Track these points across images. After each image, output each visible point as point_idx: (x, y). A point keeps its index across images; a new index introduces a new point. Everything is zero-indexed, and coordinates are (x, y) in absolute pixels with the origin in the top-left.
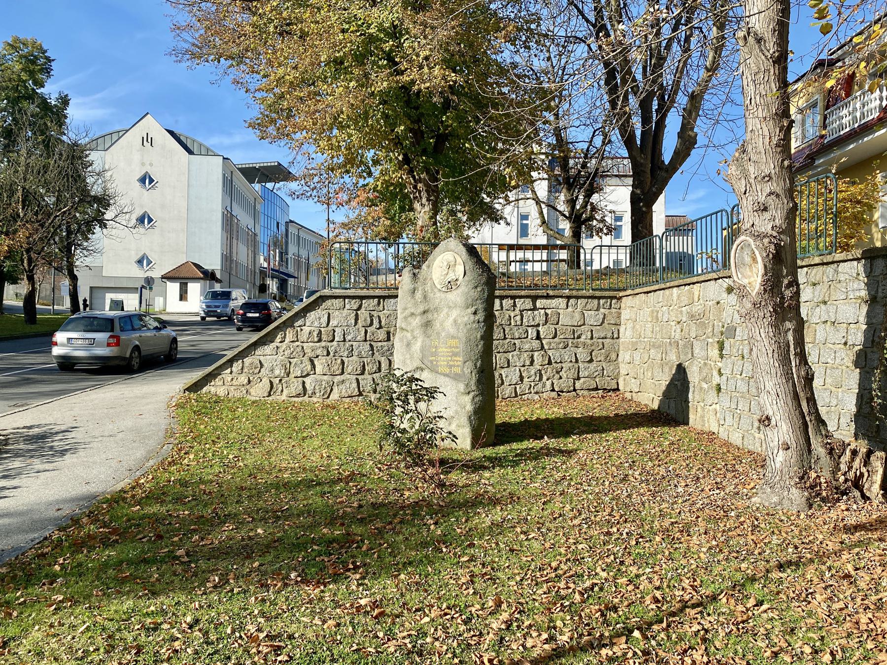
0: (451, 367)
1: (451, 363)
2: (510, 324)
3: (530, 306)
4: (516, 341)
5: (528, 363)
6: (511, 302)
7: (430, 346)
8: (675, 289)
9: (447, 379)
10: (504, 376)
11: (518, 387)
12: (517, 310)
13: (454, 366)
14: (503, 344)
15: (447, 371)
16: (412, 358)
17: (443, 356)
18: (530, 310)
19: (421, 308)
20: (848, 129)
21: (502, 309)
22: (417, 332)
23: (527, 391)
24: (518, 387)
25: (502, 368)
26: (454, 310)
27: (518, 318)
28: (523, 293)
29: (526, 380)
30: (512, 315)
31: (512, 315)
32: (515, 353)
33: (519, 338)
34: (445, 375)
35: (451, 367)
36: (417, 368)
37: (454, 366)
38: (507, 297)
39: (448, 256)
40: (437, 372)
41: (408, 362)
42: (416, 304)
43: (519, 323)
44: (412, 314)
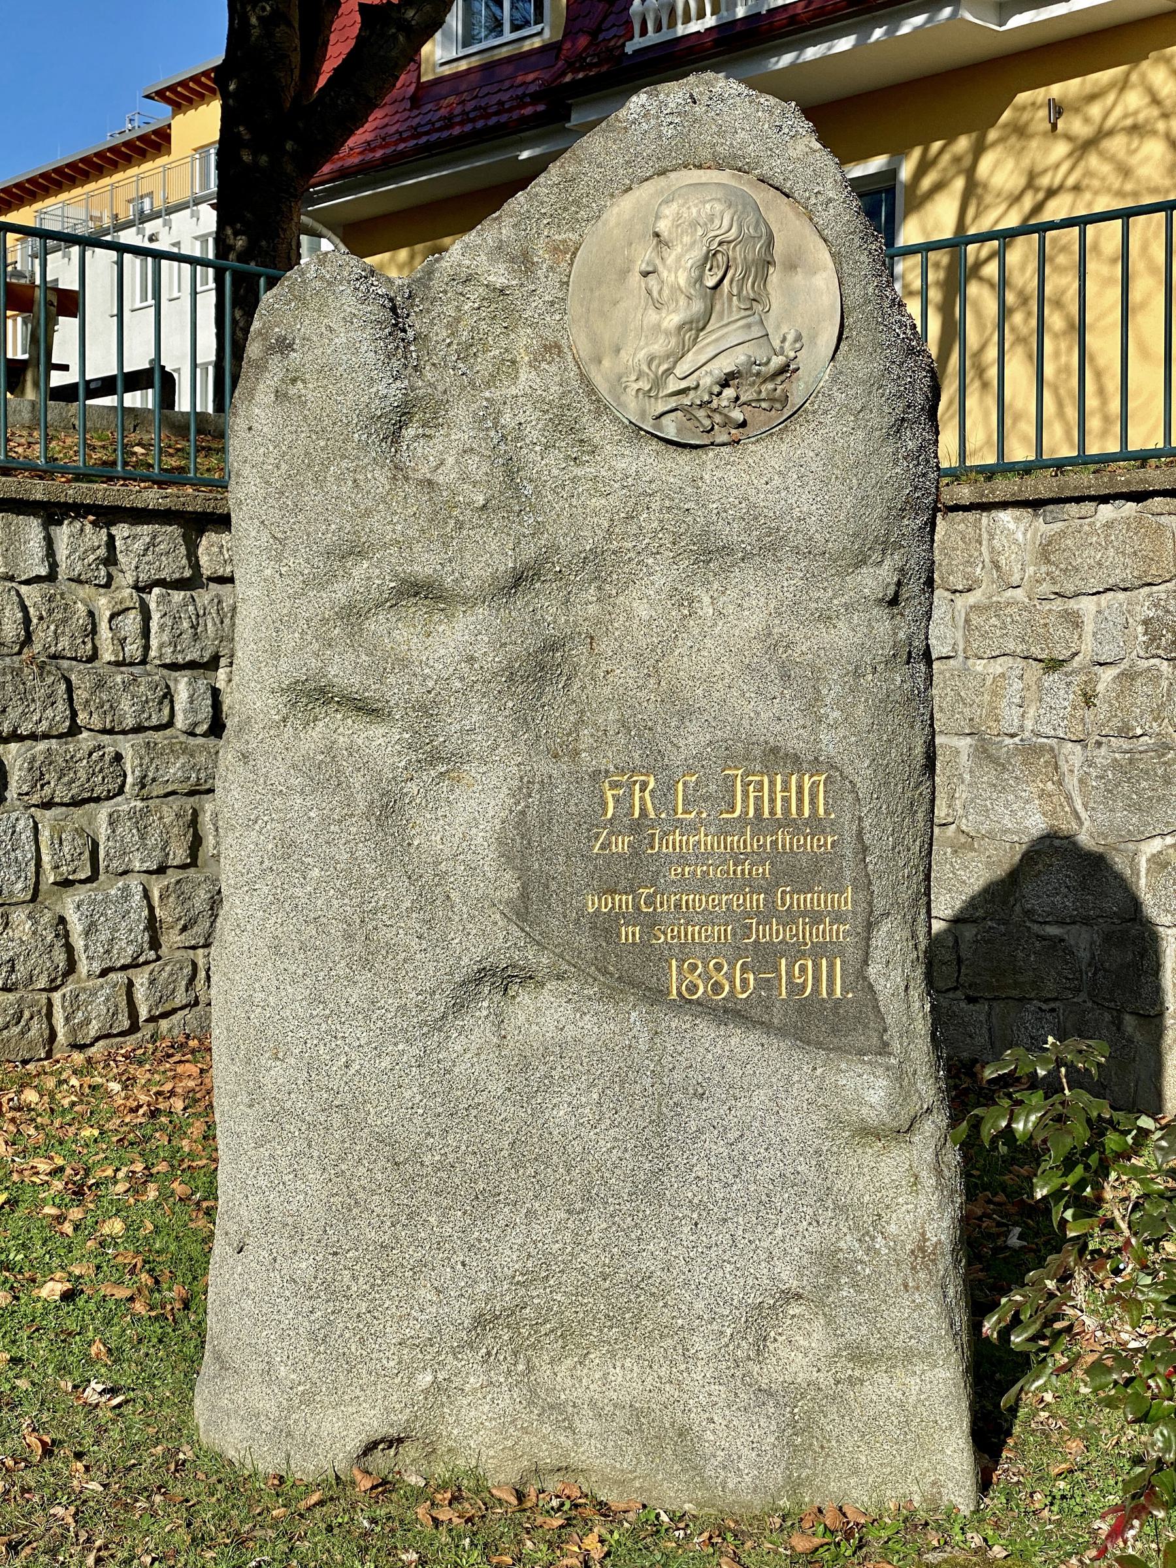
0: (765, 957)
1: (775, 933)
2: (94, 657)
3: (174, 566)
4: (127, 746)
5: (179, 853)
6: (96, 537)
7: (590, 822)
8: (1006, 517)
9: (741, 1041)
10: (76, 926)
11: (141, 979)
12: (125, 580)
13: (796, 952)
14: (71, 762)
15: (739, 983)
16: (430, 900)
17: (705, 885)
18: (180, 584)
19: (489, 555)
20: (710, 21)
21: (51, 577)
22: (469, 720)
23: (181, 998)
24: (141, 979)
25: (66, 883)
26: (745, 577)
27: (131, 623)
28: (152, 498)
29: (171, 939)
30: (104, 605)
31: (104, 605)
32: (123, 805)
33: (138, 729)
34: (730, 1014)
35: (765, 957)
36: (481, 976)
37: (796, 952)
38: (78, 510)
39: (687, 213)
40: (655, 996)
41: (401, 933)
42: (442, 513)
43: (133, 649)
44: (418, 592)
